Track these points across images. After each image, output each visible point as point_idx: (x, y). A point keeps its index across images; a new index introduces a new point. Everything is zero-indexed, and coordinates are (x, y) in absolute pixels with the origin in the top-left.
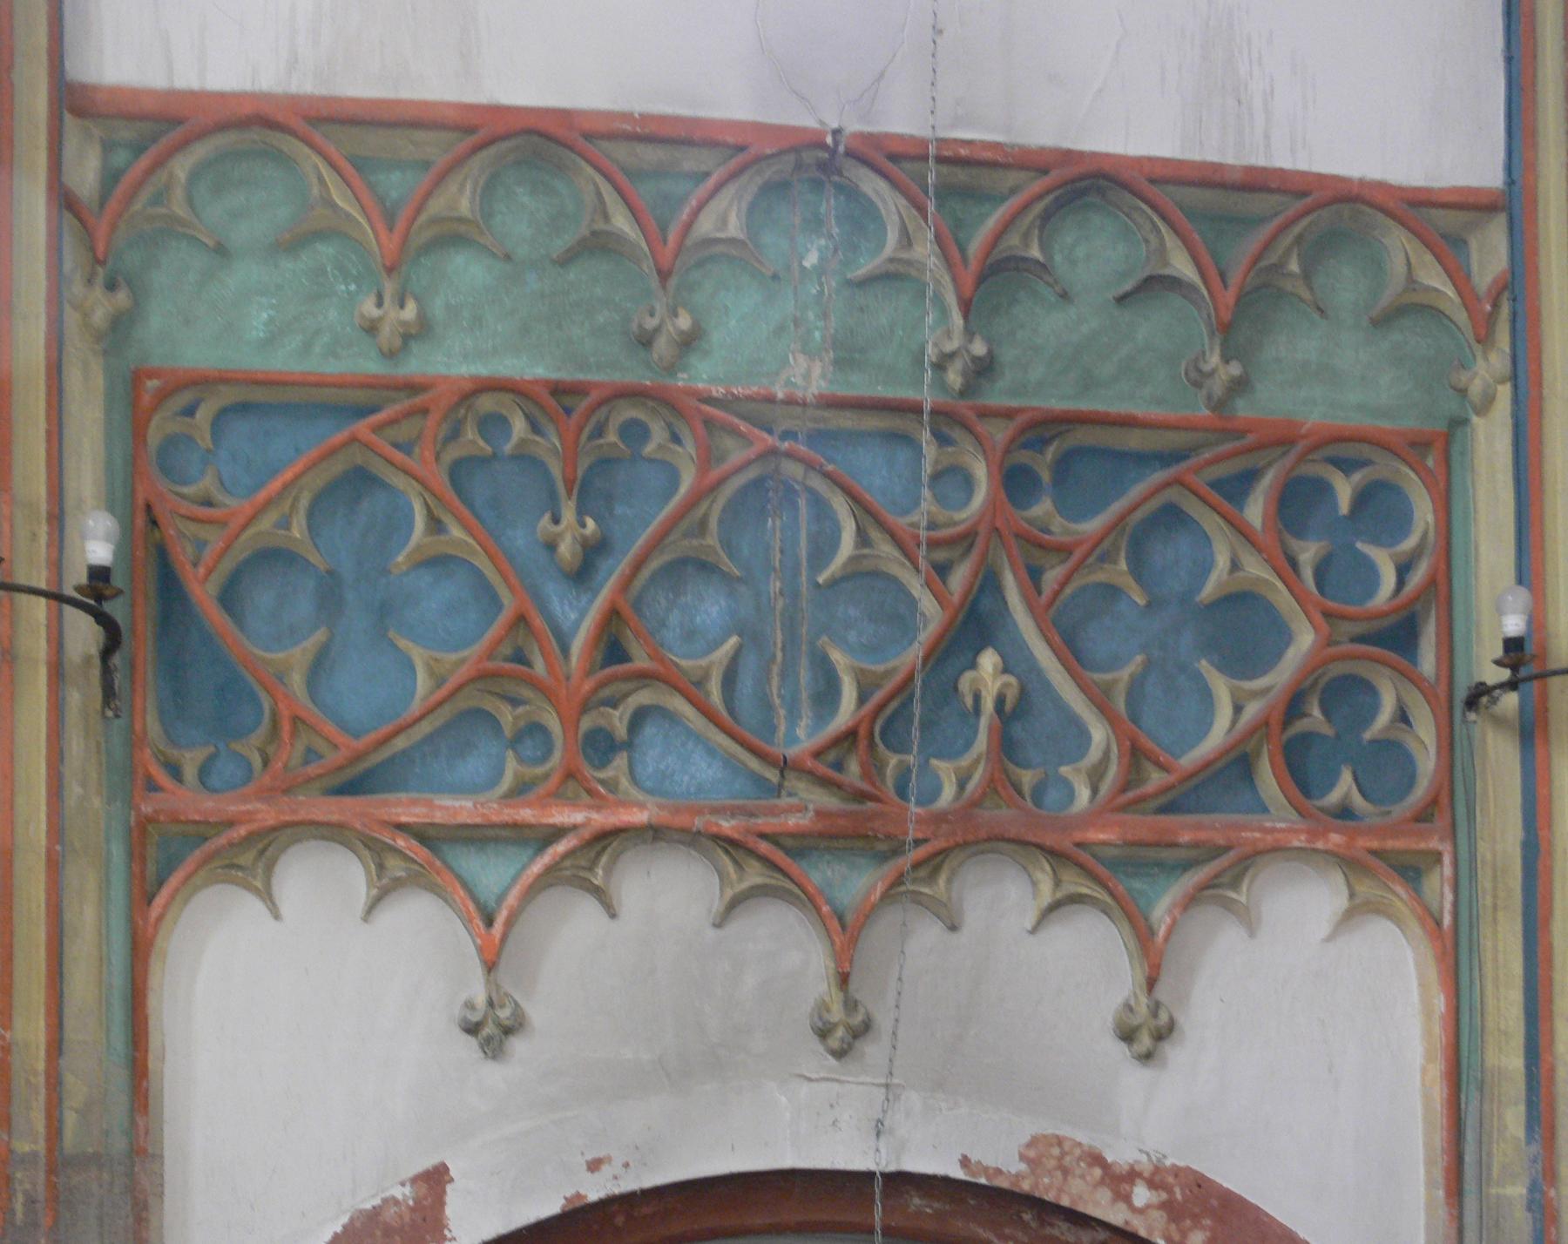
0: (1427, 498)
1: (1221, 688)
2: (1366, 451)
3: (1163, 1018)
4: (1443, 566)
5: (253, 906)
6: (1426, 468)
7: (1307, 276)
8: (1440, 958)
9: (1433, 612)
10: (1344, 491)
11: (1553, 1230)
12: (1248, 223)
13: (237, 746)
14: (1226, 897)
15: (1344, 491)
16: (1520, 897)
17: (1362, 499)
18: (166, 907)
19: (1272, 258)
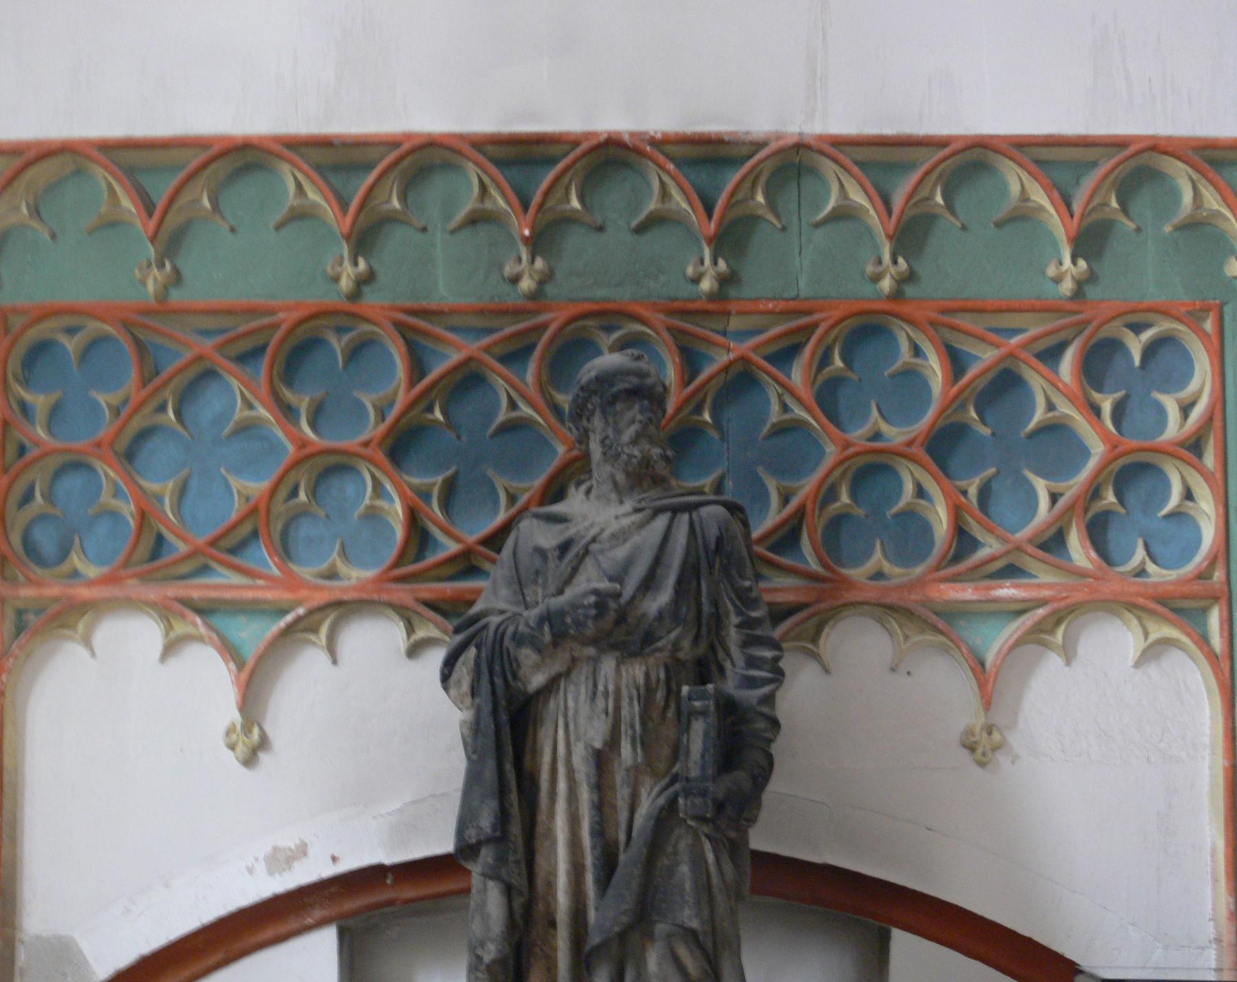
0: (1206, 356)
1: (1041, 487)
2: (1150, 317)
3: (996, 736)
4: (1219, 406)
5: (81, 651)
6: (1204, 331)
7: (950, 206)
8: (1221, 686)
9: (1212, 436)
10: (1135, 346)
11: (94, 976)
12: (905, 167)
13: (1096, 396)
14: (772, 673)
15: (1135, 346)
16: (1201, 654)
17: (1150, 351)
18: (950, 548)
19: (924, 193)
